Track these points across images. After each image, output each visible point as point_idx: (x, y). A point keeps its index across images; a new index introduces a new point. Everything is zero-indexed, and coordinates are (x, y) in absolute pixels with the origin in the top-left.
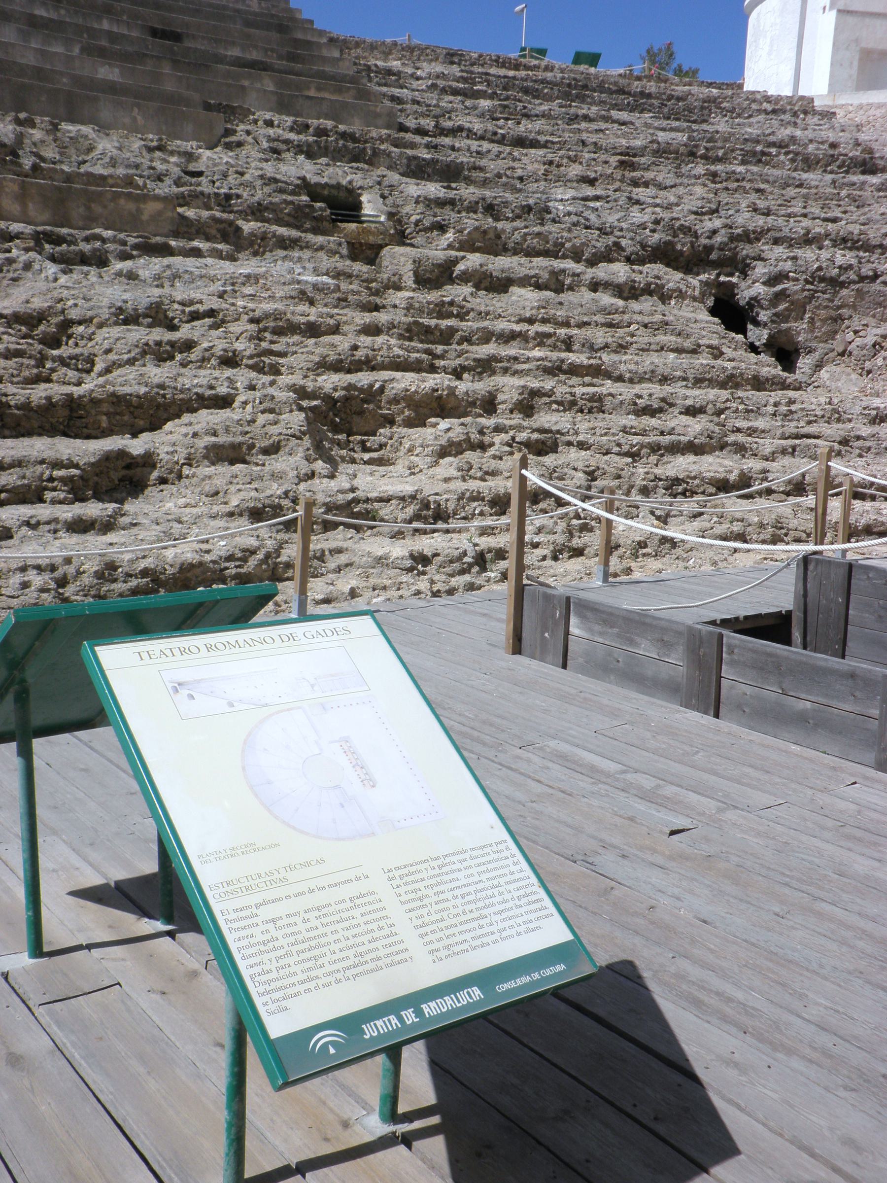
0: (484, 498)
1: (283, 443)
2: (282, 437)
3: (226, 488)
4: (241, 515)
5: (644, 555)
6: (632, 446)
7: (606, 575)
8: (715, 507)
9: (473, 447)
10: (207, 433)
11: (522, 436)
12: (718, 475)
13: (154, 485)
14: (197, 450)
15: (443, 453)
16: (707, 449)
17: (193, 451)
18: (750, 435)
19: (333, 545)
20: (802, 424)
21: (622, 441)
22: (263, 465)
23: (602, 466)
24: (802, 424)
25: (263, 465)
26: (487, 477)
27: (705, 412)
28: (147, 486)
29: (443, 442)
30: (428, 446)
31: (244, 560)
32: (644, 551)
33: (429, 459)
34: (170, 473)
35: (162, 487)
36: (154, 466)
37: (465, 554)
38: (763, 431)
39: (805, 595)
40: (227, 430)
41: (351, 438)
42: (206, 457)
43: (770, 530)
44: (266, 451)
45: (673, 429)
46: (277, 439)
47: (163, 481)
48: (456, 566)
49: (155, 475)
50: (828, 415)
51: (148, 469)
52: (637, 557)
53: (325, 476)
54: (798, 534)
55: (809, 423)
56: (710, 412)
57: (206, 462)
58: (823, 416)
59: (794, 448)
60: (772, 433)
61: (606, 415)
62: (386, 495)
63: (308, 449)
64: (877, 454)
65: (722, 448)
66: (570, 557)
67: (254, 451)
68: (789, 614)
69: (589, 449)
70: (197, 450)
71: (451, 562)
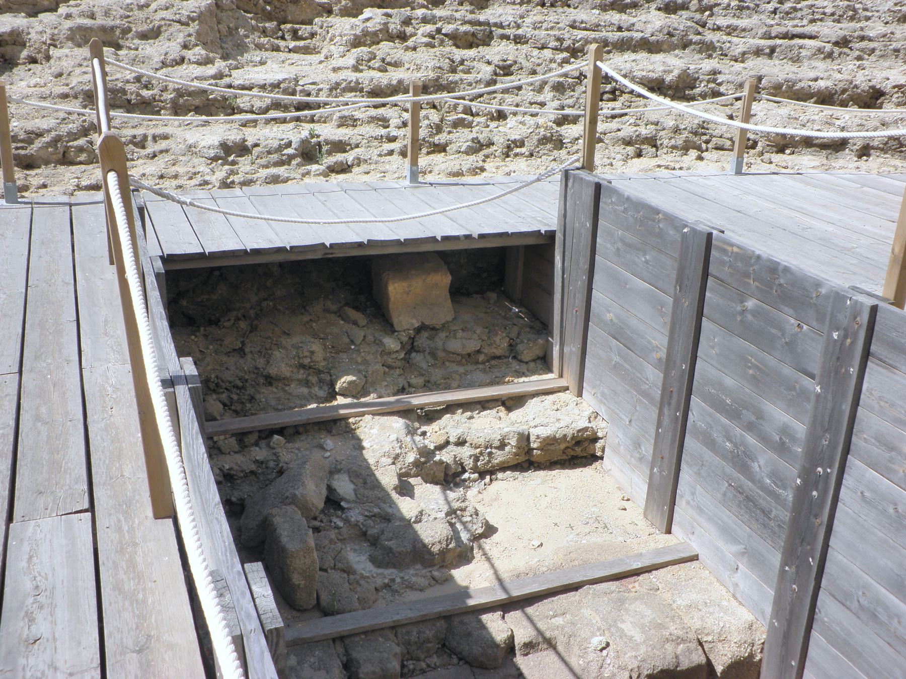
0: (363, 88)
1: (163, 29)
2: (163, 23)
3: (70, 69)
4: (76, 97)
5: (516, 155)
6: (575, 41)
7: (414, 176)
8: (636, 107)
9: (391, 38)
10: (82, 14)
11: (448, 28)
12: (651, 75)
13: (24, 63)
14: (60, 31)
15: (357, 42)
16: (665, 47)
17: (56, 31)
18: (729, 34)
19: (159, 131)
20: (805, 22)
21: (566, 36)
22: (137, 49)
23: (520, 60)
24: (805, 22)
25: (137, 49)
26: (389, 68)
27: (688, 9)
28: (17, 65)
29: (358, 32)
30: (345, 35)
31: (30, 142)
32: (518, 150)
33: (342, 49)
34: (38, 53)
35: (32, 66)
36: (24, 45)
37: (289, 145)
38: (744, 30)
39: (565, 216)
40: (107, 13)
41: (282, 27)
42: (70, 38)
43: (685, 134)
44: (144, 36)
45: (633, 25)
46: (157, 23)
47: (34, 61)
48: (275, 157)
49: (24, 53)
50: (839, 13)
51: (19, 48)
52: (508, 156)
53: (194, 63)
54: (720, 142)
55: (813, 21)
56: (693, 8)
57: (70, 44)
58: (833, 14)
59: (773, 50)
60: (753, 32)
61: (571, 10)
62: (247, 82)
63: (190, 35)
64: (881, 56)
65: (685, 47)
66: (428, 153)
67: (130, 35)
68: (551, 235)
69: (527, 42)
70: (60, 31)
71: (269, 153)
